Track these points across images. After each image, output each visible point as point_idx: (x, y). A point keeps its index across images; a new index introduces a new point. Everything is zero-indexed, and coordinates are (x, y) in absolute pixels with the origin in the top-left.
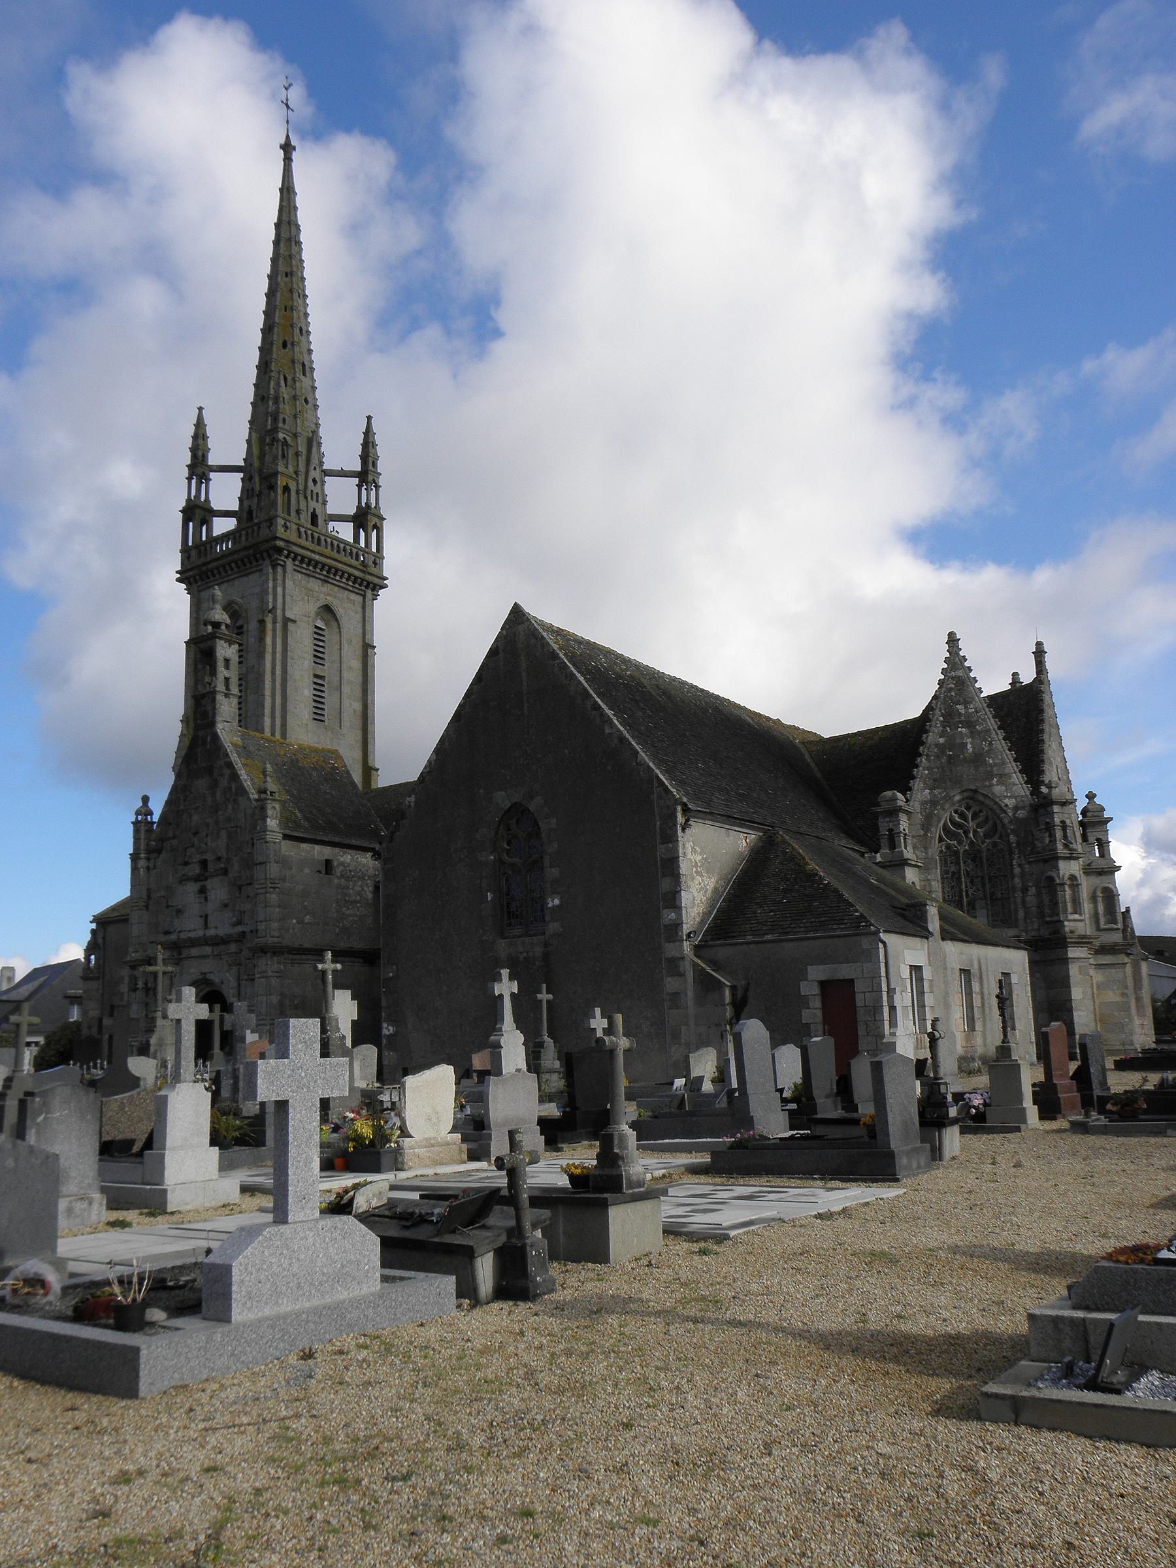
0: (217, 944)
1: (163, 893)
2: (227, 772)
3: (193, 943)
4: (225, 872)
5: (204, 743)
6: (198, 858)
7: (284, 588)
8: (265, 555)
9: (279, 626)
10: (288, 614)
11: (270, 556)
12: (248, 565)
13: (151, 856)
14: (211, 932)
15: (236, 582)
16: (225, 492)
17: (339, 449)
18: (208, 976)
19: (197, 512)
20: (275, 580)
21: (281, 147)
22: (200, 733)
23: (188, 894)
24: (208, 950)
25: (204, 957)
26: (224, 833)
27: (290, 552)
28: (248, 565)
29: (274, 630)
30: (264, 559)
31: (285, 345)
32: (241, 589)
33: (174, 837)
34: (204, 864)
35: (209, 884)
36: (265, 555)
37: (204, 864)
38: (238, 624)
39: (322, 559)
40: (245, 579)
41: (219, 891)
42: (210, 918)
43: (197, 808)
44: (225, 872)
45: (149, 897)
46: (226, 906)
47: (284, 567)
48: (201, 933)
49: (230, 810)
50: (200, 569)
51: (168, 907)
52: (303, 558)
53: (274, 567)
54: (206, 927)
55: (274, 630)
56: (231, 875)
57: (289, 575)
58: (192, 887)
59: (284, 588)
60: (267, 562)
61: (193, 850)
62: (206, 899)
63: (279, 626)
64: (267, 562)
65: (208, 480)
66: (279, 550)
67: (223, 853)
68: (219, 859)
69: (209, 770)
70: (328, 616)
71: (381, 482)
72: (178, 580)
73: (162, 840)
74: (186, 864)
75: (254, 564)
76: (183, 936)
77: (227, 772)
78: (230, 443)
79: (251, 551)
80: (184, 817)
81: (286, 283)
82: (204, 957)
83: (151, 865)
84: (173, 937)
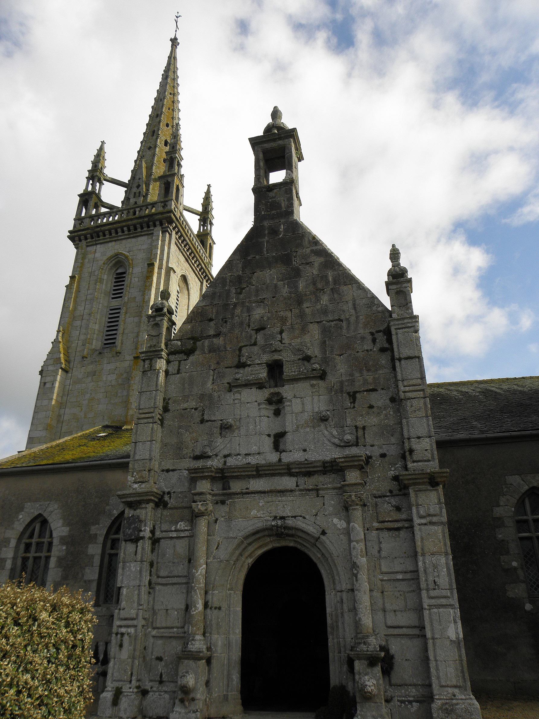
0: (309, 474)
1: (193, 404)
2: (318, 261)
3: (259, 472)
4: (322, 376)
5: (274, 232)
6: (266, 358)
7: (169, 248)
8: (158, 223)
9: (163, 271)
10: (170, 266)
11: (161, 224)
12: (139, 230)
13: (172, 358)
14: (287, 458)
15: (124, 241)
16: (113, 196)
17: (191, 197)
18: (290, 522)
19: (88, 199)
20: (163, 241)
21: (171, 40)
22: (266, 223)
23: (249, 407)
24: (288, 482)
25: (282, 492)
26: (315, 331)
27: (176, 226)
28: (139, 230)
29: (159, 274)
30: (155, 226)
31: (167, 125)
32: (131, 247)
33: (217, 335)
34: (275, 369)
35: (287, 391)
36: (158, 223)
37: (275, 369)
38: (120, 271)
39: (190, 243)
40: (133, 240)
41: (304, 401)
42: (289, 437)
43: (262, 301)
44: (322, 376)
45: (166, 409)
46: (324, 419)
47: (170, 235)
48: (273, 457)
49: (325, 299)
50: (83, 235)
51: (202, 421)
52: (182, 235)
53: (164, 232)
54: (276, 447)
55: (159, 274)
56: (332, 379)
57: (173, 240)
58: (252, 397)
59: (169, 248)
60: (159, 228)
61: (255, 349)
62: (277, 413)
63: (163, 271)
64: (159, 228)
65: (101, 184)
66: (171, 222)
67: (315, 351)
68: (307, 359)
69: (286, 260)
70: (183, 285)
71: (213, 221)
72: (68, 237)
73: (195, 339)
74: (241, 365)
75: (145, 229)
76: (231, 462)
77: (318, 261)
78: (121, 165)
79: (146, 219)
80: (238, 311)
81: (170, 97)
82: (282, 492)
83: (173, 368)
84: (215, 463)
